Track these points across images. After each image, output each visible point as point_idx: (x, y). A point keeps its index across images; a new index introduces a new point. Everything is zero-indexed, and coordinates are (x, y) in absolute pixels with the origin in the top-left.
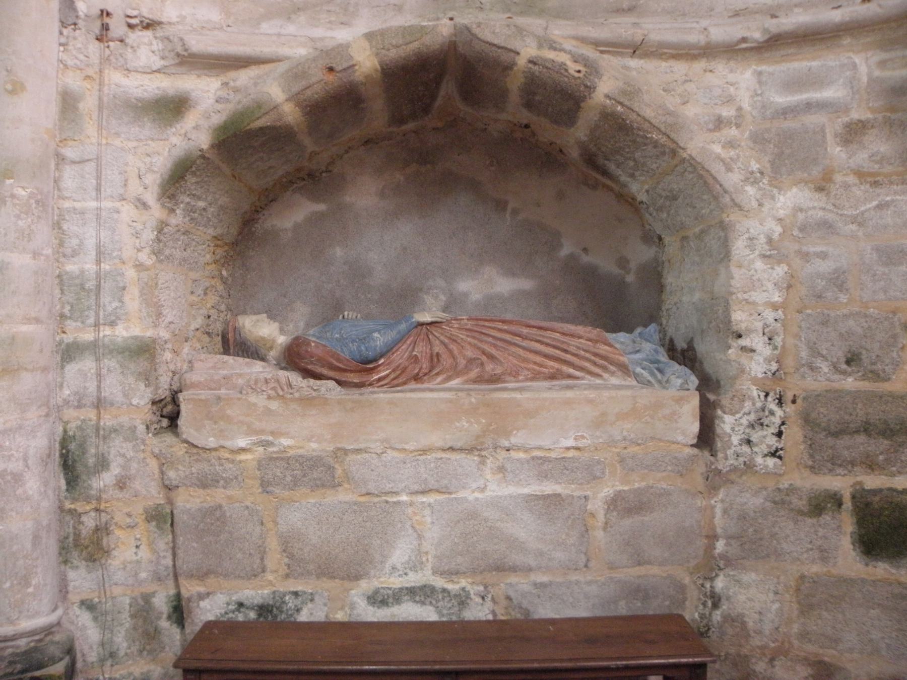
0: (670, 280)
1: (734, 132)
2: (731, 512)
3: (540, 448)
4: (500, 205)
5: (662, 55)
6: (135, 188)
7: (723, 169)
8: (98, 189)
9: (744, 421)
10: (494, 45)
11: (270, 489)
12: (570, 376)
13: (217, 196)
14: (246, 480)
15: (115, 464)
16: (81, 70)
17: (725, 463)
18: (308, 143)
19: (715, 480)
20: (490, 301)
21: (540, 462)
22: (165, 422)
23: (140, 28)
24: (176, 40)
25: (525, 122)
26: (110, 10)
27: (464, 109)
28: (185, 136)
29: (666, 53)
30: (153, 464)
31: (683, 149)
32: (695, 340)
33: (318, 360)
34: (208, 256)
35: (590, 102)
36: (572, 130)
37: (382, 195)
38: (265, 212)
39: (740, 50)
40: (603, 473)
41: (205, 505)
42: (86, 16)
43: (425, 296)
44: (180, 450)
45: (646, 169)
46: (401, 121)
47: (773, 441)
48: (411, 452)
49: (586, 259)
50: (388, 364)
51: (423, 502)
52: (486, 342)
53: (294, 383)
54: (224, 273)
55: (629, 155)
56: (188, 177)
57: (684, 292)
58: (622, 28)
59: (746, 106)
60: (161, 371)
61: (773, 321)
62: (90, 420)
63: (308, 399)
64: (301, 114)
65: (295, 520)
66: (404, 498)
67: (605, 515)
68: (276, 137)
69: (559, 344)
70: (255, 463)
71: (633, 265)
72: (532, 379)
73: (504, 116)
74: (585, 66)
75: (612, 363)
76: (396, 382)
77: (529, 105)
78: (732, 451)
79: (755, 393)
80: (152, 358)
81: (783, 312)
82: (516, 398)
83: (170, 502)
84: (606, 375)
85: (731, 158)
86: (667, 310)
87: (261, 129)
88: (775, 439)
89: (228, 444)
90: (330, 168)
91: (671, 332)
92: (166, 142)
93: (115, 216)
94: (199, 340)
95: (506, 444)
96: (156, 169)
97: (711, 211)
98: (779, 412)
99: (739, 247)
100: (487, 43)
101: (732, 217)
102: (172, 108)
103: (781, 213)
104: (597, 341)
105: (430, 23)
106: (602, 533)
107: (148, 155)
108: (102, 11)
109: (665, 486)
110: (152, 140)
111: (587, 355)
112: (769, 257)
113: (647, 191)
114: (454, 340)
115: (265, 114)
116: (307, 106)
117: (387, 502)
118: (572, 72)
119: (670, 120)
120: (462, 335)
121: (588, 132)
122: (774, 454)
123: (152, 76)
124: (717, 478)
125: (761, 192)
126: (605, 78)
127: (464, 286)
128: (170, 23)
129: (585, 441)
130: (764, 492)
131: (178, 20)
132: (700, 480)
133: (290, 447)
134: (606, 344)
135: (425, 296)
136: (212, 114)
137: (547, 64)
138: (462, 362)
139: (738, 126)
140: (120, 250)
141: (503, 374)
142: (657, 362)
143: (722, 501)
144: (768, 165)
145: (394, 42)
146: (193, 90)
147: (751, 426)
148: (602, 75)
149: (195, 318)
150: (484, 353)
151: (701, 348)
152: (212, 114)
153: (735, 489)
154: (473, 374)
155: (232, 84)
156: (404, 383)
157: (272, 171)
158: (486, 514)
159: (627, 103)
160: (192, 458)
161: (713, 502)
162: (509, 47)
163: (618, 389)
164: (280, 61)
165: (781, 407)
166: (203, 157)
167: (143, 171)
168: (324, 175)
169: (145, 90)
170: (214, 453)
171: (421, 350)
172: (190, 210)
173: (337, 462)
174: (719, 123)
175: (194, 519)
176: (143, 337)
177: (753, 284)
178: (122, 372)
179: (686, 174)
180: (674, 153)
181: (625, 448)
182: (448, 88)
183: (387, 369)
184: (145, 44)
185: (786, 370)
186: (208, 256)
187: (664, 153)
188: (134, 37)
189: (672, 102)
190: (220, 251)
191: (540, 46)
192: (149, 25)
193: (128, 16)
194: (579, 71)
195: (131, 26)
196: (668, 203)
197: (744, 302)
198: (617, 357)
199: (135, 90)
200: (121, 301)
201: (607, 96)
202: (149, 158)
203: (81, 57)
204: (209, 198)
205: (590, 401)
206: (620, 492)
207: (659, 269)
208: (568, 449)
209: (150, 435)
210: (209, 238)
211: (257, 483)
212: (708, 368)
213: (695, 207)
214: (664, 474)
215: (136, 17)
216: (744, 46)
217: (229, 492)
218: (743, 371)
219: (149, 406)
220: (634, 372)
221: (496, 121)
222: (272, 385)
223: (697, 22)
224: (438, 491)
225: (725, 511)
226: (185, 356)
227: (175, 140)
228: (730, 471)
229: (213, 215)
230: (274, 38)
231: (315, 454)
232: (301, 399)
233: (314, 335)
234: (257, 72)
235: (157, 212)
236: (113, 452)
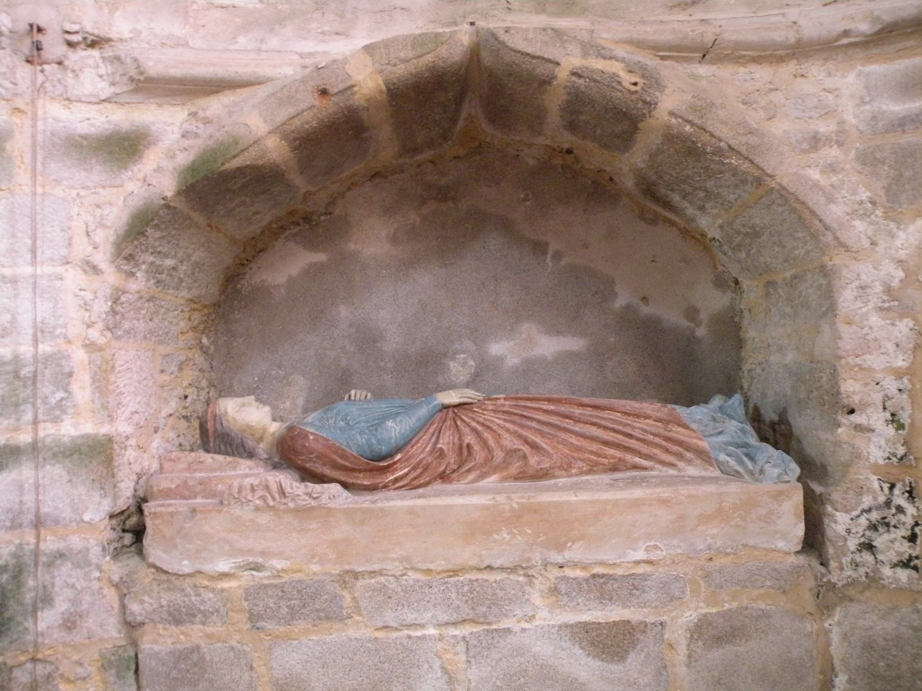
0: (751, 333)
1: (833, 153)
2: (852, 639)
3: (602, 563)
4: (539, 248)
5: (739, 57)
6: (82, 248)
7: (822, 200)
8: (34, 252)
9: (863, 521)
10: (528, 54)
11: (261, 624)
12: (636, 467)
13: (190, 251)
14: (230, 613)
15: (61, 598)
16: (7, 100)
17: (840, 573)
18: (300, 183)
19: (827, 597)
20: (531, 369)
21: (602, 581)
22: (128, 538)
23: (83, 46)
24: (128, 61)
25: (566, 146)
26: (42, 25)
27: (488, 129)
28: (145, 181)
29: (744, 56)
30: (111, 595)
31: (771, 176)
32: (790, 411)
33: (317, 457)
34: (182, 324)
35: (651, 122)
36: (627, 155)
37: (394, 240)
38: (253, 265)
39: (842, 46)
40: (683, 592)
41: (178, 646)
42: (11, 32)
43: (451, 364)
44: (145, 576)
45: (720, 201)
46: (415, 151)
47: (905, 548)
48: (439, 573)
49: (645, 310)
50: (406, 460)
51: (455, 636)
52: (530, 428)
53: (288, 490)
54: (205, 341)
55: (697, 185)
56: (149, 231)
57: (773, 352)
58: (683, 25)
59: (850, 118)
60: (120, 475)
61: (896, 392)
62: (28, 544)
63: (305, 510)
64: (287, 148)
65: (293, 662)
66: (432, 631)
67: (688, 646)
68: (258, 180)
69: (620, 428)
70: (241, 591)
71: (704, 316)
72: (589, 472)
73: (540, 141)
74: (643, 76)
75: (688, 448)
76: (416, 483)
77: (572, 127)
78: (849, 559)
79: (876, 485)
80: (109, 461)
81: (909, 380)
82: (569, 502)
83: (134, 643)
84: (681, 464)
85: (832, 186)
86: (750, 371)
87: (239, 169)
88: (907, 544)
89: (207, 568)
90: (330, 210)
91: (755, 398)
92: (120, 189)
93: (58, 284)
94: (173, 428)
95: (560, 559)
96: (109, 224)
97: (808, 252)
98: (910, 510)
99: (847, 299)
100: (519, 52)
101: (837, 261)
102: (123, 147)
103: (902, 254)
104: (668, 422)
105: (447, 30)
106: (684, 669)
107: (98, 206)
108: (31, 26)
109: (763, 606)
110: (103, 187)
111: (657, 440)
112: (888, 309)
113: (721, 227)
114: (488, 427)
115: (242, 151)
116: (295, 140)
117: (409, 637)
118: (626, 84)
119: (753, 140)
120: (498, 421)
121: (646, 158)
122: (906, 564)
123: (100, 106)
124: (831, 593)
125: (873, 227)
126: (668, 91)
127: (496, 348)
128: (121, 40)
129: (659, 552)
130: (897, 614)
131: (131, 35)
132: (808, 598)
133: (284, 571)
134: (679, 425)
135: (451, 364)
136: (177, 152)
137: (595, 76)
138: (499, 455)
139: (840, 144)
140: (65, 326)
141: (552, 468)
142: (746, 445)
143: (839, 624)
144: (882, 193)
145: (402, 55)
146: (153, 123)
147: (873, 527)
148: (665, 87)
149: (166, 401)
150: (526, 441)
151: (800, 423)
152: (177, 152)
153: (854, 608)
154: (514, 469)
155: (201, 114)
156: (426, 484)
157: (258, 217)
158: (536, 649)
159: (696, 121)
160: (162, 587)
161: (826, 625)
162: (546, 56)
163: (699, 484)
164: (260, 83)
165: (914, 502)
166: (167, 206)
167: (92, 226)
168: (323, 218)
169: (93, 125)
170: (188, 580)
171: (446, 441)
172: (155, 271)
173: (345, 587)
174: (815, 142)
175: (163, 664)
176: (96, 435)
177: (866, 346)
178: (70, 481)
179: (774, 206)
180: (759, 182)
181: (711, 559)
182: (472, 109)
183: (406, 467)
184: (90, 66)
185: (918, 456)
186: (182, 324)
187: (744, 182)
188: (75, 57)
189: (754, 117)
190: (196, 316)
191: (585, 55)
192: (94, 43)
193: (68, 32)
194: (635, 84)
195: (70, 44)
196: (748, 241)
197: (856, 369)
198: (695, 441)
199: (79, 124)
200: (66, 391)
201: (671, 114)
202: (99, 211)
203: (7, 84)
204: (180, 255)
205: (664, 502)
206: (705, 615)
207: (737, 319)
208: (638, 563)
209: (108, 558)
210: (182, 302)
211: (244, 617)
212: (811, 450)
213: (785, 247)
214: (762, 591)
215: (76, 32)
216: (845, 41)
217: (209, 630)
218: (858, 456)
219: (107, 520)
220: (717, 460)
221: (530, 145)
222: (260, 493)
223: (783, 15)
224: (473, 621)
225: (845, 637)
226: (154, 451)
227: (131, 186)
228: (848, 584)
229: (185, 274)
230: (253, 55)
231: (316, 578)
232: (297, 511)
233: (312, 424)
234: (232, 98)
235: (111, 277)
236: (58, 582)
